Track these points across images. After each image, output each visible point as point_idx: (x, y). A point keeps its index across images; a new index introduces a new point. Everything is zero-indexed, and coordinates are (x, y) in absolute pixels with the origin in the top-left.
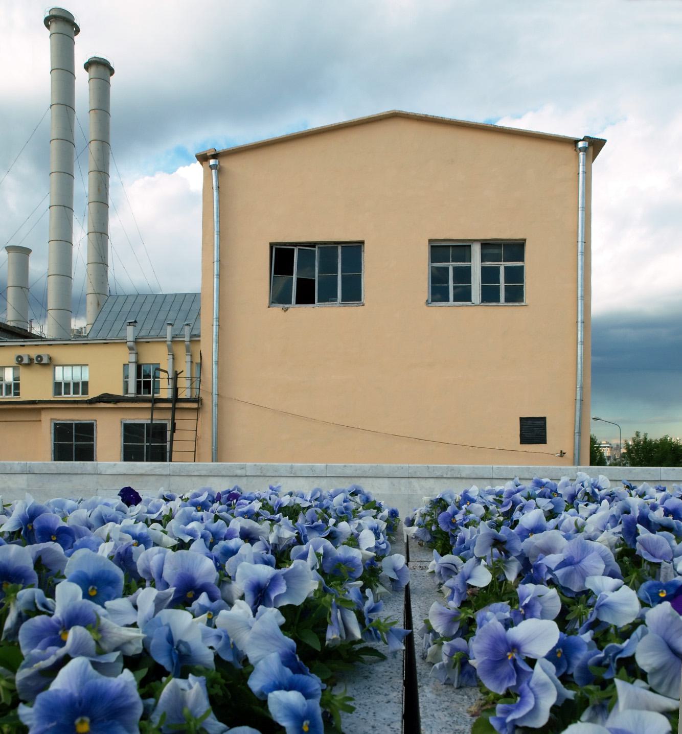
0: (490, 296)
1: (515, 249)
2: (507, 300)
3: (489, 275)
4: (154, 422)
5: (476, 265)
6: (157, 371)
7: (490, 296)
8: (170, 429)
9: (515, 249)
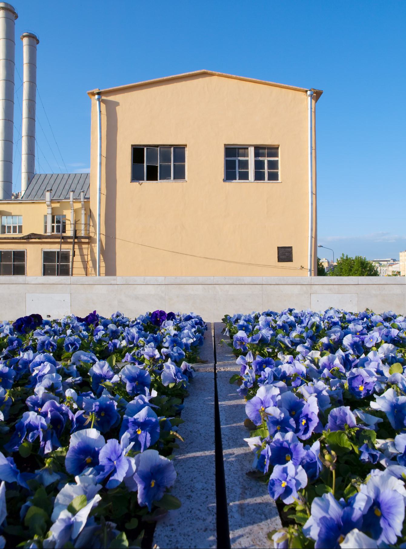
0: (259, 176)
1: (273, 151)
2: (269, 179)
3: (259, 165)
4: (62, 250)
5: (251, 159)
6: (176, 150)
7: (259, 176)
8: (313, 270)
9: (273, 151)
